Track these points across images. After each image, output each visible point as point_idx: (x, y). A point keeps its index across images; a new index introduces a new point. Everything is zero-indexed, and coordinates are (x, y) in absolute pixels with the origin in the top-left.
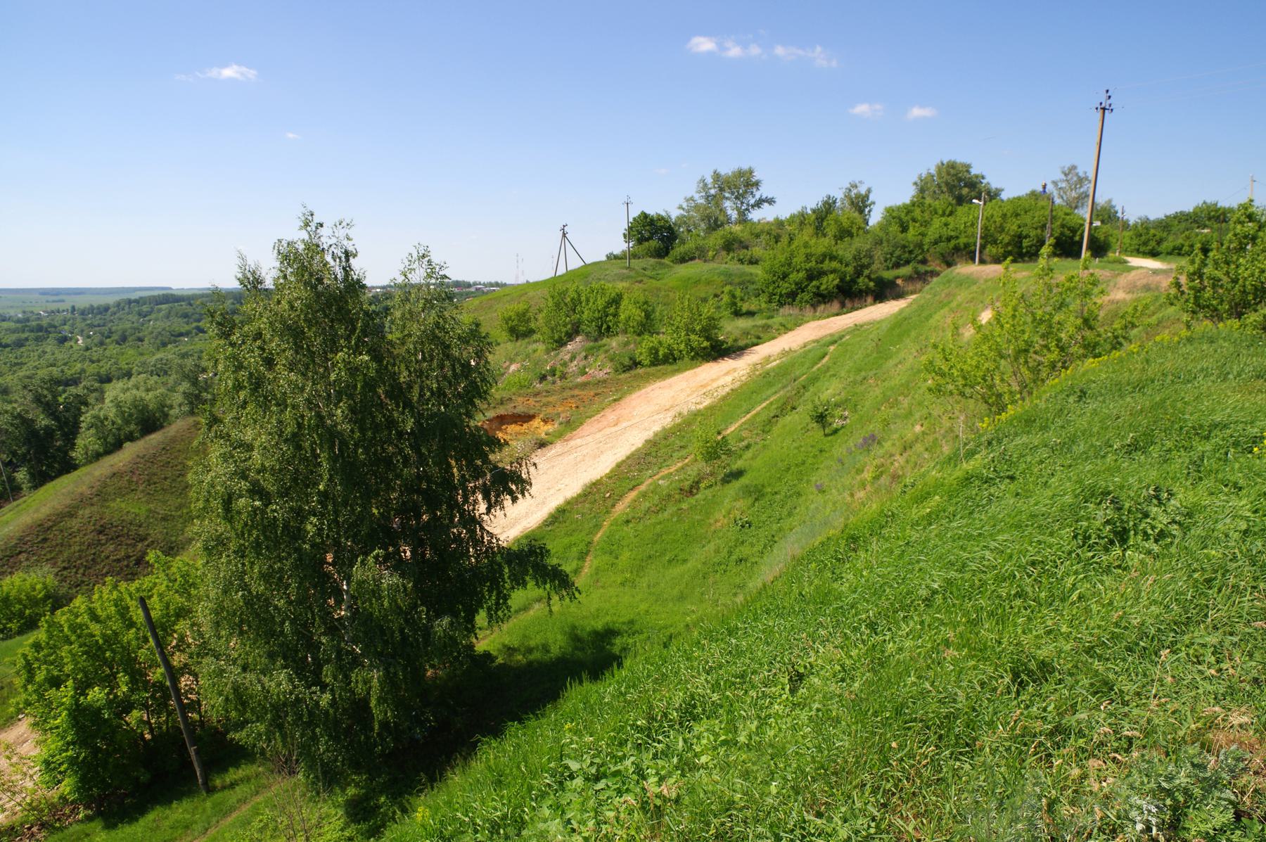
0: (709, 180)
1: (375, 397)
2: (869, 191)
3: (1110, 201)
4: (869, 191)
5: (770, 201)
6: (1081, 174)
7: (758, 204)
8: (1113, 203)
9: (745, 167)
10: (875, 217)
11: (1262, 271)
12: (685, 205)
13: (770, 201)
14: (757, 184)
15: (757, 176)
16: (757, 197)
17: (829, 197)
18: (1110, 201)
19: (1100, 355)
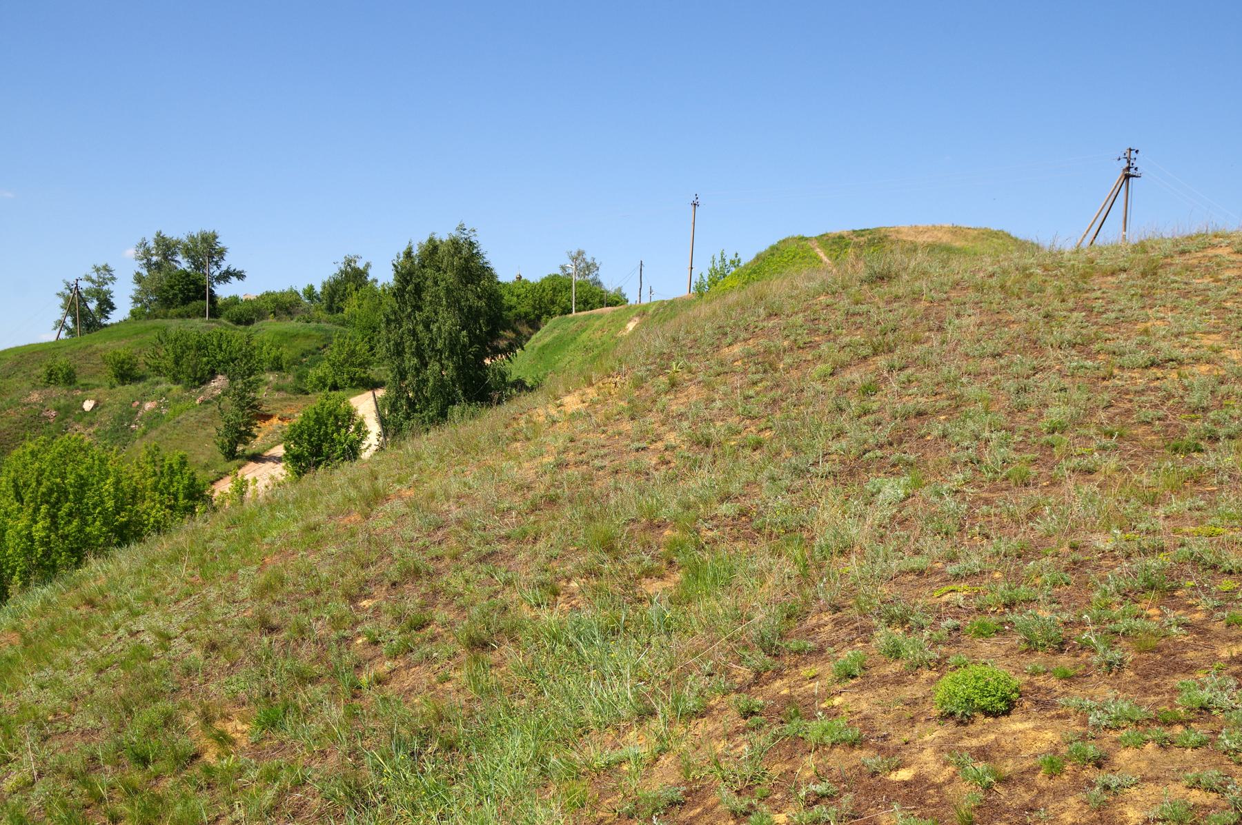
0: (152, 244)
1: (488, 388)
2: (368, 265)
3: (620, 289)
4: (368, 265)
5: (240, 276)
6: (589, 260)
7: (226, 276)
8: (623, 291)
9: (209, 229)
10: (145, 272)
11: (115, 819)
12: (94, 276)
13: (240, 276)
14: (221, 253)
15: (223, 242)
16: (224, 268)
17: (167, 247)
18: (620, 289)
19: (912, 242)
